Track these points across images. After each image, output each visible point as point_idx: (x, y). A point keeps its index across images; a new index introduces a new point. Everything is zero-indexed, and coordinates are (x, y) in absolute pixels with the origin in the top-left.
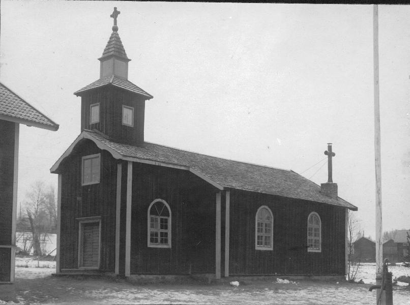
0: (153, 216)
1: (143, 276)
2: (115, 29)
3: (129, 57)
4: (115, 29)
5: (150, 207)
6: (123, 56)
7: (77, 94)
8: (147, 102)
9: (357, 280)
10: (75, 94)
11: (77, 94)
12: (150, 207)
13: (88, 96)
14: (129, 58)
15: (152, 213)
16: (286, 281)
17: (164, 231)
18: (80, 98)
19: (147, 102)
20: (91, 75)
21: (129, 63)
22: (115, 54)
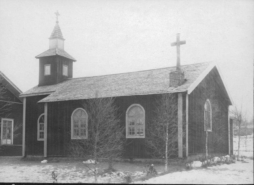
0: (41, 123)
1: (35, 156)
2: (57, 22)
3: (64, 38)
4: (57, 22)
5: (39, 119)
6: (208, 78)
7: (37, 58)
8: (74, 62)
9: (56, 178)
10: (76, 61)
11: (37, 58)
12: (39, 119)
13: (45, 60)
14: (64, 38)
15: (40, 122)
16: (93, 162)
17: (76, 128)
18: (38, 60)
19: (74, 62)
20: (44, 47)
21: (65, 41)
22: (57, 35)
